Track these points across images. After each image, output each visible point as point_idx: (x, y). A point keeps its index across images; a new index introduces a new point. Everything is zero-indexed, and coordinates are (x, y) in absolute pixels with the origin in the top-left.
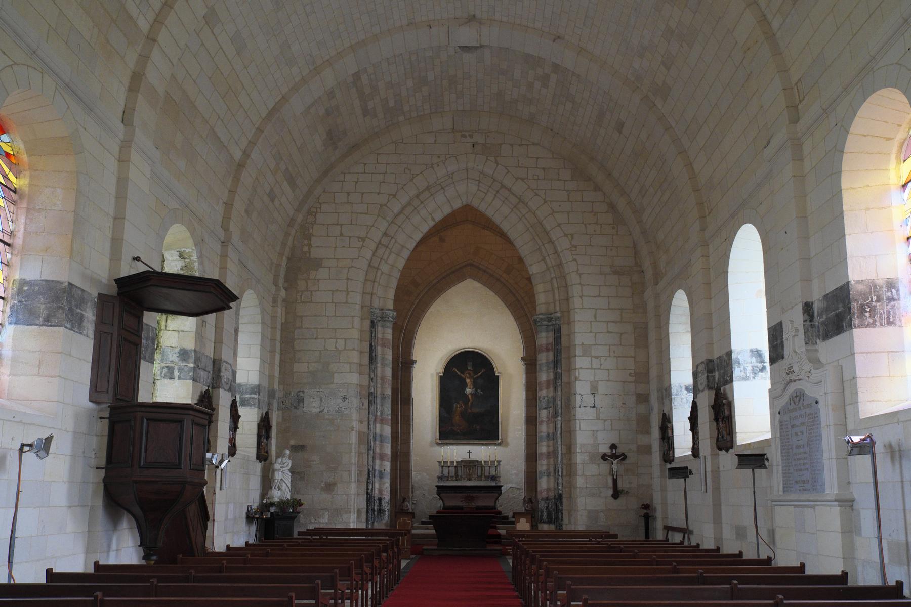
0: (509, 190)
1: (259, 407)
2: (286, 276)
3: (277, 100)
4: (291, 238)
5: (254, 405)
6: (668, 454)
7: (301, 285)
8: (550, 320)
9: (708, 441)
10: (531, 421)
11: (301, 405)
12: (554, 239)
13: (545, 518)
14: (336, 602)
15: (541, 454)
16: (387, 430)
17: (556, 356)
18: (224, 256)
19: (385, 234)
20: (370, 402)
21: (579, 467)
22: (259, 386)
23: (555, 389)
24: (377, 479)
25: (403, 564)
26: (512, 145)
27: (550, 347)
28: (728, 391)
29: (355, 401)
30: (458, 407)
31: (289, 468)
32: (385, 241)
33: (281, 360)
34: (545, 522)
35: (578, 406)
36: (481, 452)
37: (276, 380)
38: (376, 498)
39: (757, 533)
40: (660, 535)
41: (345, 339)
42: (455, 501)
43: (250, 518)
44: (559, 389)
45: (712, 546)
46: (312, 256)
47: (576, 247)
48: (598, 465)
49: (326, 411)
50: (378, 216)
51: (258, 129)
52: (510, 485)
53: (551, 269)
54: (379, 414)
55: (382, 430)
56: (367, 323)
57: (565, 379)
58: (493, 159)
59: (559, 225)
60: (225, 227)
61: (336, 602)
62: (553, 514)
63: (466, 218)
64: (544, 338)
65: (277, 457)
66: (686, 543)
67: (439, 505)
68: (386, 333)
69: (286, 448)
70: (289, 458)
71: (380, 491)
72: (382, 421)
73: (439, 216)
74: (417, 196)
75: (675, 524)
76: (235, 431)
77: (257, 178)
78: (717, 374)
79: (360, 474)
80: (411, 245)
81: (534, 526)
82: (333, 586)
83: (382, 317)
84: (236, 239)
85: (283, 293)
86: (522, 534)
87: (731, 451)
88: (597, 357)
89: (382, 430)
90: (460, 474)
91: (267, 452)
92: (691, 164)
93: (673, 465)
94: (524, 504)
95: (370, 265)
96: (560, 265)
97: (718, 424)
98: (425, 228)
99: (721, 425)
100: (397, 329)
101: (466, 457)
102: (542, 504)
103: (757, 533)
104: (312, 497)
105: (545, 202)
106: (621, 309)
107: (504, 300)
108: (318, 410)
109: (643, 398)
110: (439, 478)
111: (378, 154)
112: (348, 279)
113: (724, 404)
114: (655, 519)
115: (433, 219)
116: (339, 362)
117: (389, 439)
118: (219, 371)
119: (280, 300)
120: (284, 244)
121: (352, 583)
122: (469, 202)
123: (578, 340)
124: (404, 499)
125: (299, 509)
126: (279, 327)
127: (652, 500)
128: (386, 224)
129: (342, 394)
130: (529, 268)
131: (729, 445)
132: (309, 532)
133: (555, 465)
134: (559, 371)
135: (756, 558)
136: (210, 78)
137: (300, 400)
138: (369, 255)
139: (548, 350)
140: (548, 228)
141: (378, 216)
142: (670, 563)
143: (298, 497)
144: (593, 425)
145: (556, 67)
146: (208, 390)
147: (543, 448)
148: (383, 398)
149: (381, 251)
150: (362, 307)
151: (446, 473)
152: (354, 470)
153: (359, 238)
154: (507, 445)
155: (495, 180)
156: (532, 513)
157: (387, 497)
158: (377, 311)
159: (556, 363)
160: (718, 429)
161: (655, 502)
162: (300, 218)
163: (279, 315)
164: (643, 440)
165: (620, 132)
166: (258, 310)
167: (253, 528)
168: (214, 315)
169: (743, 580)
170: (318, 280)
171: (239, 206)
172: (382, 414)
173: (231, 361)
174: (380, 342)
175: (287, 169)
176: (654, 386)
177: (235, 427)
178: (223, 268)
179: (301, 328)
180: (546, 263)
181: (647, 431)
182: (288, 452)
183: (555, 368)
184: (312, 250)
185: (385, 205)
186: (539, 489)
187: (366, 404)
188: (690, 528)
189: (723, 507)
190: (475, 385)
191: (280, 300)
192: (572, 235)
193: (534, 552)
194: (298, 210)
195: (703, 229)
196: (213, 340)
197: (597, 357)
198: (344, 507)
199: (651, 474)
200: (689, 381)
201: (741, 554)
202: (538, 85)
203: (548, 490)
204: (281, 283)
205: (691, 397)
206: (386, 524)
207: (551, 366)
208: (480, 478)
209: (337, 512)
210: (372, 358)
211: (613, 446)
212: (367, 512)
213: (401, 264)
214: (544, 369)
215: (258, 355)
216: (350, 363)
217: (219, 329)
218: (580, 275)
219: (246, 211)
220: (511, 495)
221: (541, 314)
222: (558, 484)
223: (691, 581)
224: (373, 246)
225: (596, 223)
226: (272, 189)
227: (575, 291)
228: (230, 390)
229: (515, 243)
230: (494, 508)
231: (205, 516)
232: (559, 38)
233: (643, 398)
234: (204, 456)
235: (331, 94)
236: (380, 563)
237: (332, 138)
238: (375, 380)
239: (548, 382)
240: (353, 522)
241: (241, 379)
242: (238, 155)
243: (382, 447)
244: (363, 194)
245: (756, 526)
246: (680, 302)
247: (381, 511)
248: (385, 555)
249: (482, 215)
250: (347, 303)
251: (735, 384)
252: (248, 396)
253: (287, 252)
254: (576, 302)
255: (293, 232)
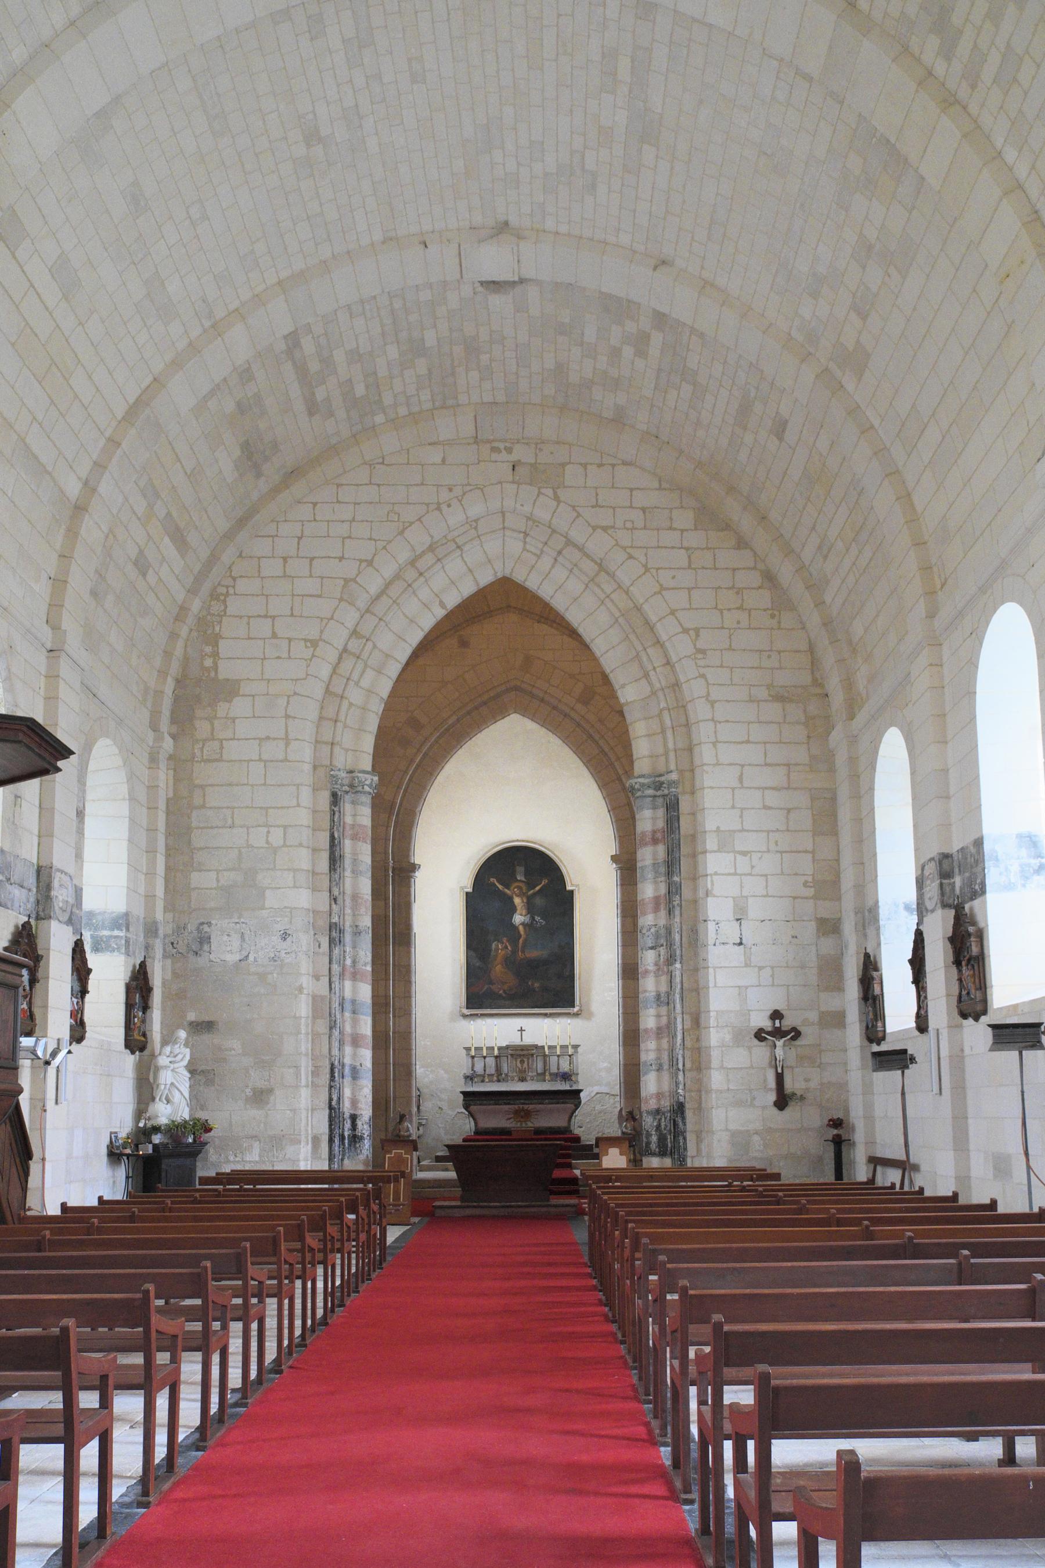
0: (581, 549)
1: (127, 954)
2: (173, 712)
3: (144, 386)
4: (180, 644)
5: (119, 949)
6: (874, 1026)
7: (202, 728)
8: (659, 786)
9: (944, 1001)
10: (630, 972)
11: (206, 947)
12: (664, 637)
13: (653, 1146)
14: (246, 1302)
15: (646, 1030)
16: (365, 992)
17: (670, 852)
18: (52, 677)
19: (355, 633)
20: (331, 941)
21: (715, 1054)
22: (127, 914)
23: (670, 912)
24: (348, 1080)
25: (393, 1234)
26: (585, 466)
27: (659, 835)
28: (977, 911)
29: (304, 940)
30: (500, 948)
31: (185, 1062)
32: (354, 645)
33: (168, 869)
34: (653, 1154)
35: (711, 942)
36: (541, 1029)
37: (160, 905)
38: (347, 1115)
39: (1029, 1167)
40: (862, 1173)
41: (285, 827)
42: (498, 1119)
43: (114, 1155)
44: (677, 912)
45: (946, 1191)
46: (221, 677)
47: (703, 652)
48: (750, 1048)
49: (251, 958)
50: (341, 600)
51: (110, 440)
52: (596, 1089)
53: (660, 694)
54: (348, 962)
55: (355, 990)
56: (325, 797)
57: (686, 893)
58: (549, 492)
59: (673, 612)
60: (53, 623)
61: (246, 1302)
62: (669, 1139)
63: (503, 603)
64: (649, 819)
65: (165, 1042)
66: (906, 1188)
67: (467, 1126)
68: (360, 815)
69: (178, 1027)
70: (186, 1045)
71: (354, 1102)
72: (355, 976)
73: (452, 600)
74: (412, 563)
75: (889, 1155)
76: (83, 997)
77: (111, 531)
78: (958, 881)
79: (315, 1073)
80: (403, 654)
81: (635, 1162)
82: (240, 1271)
83: (351, 786)
84: (73, 642)
85: (168, 744)
86: (608, 1177)
87: (983, 1019)
88: (744, 853)
89: (355, 990)
90: (505, 1069)
91: (144, 1035)
92: (909, 495)
93: (884, 1047)
94: (620, 1124)
95: (327, 691)
96: (676, 686)
97: (960, 971)
98: (428, 622)
99: (966, 972)
100: (381, 806)
101: (515, 1039)
102: (648, 1122)
103: (1029, 1167)
104: (228, 1116)
105: (647, 570)
106: (788, 765)
107: (579, 750)
108: (237, 957)
109: (830, 927)
110: (466, 1077)
111: (338, 485)
112: (287, 717)
113: (969, 935)
114: (852, 1144)
115: (442, 604)
116: (274, 869)
117: (368, 1010)
118: (49, 887)
119: (162, 757)
120: (167, 654)
121: (280, 1268)
122: (507, 573)
123: (711, 821)
124: (402, 1117)
125: (205, 1137)
126: (162, 805)
127: (847, 1111)
128: (357, 615)
129: (280, 927)
130: (619, 694)
131: (979, 1008)
132: (221, 1178)
133: (672, 1050)
134: (676, 879)
135: (1027, 1210)
136: (13, 344)
137: (204, 940)
138: (325, 672)
139: (655, 841)
140: (653, 618)
141: (341, 600)
142: (857, 1222)
143: (202, 1115)
144: (740, 973)
145: (660, 319)
146: (28, 923)
147: (649, 1020)
148: (357, 933)
149: (347, 664)
150: (315, 767)
151: (479, 1068)
152: (305, 1065)
153: (306, 640)
154: (590, 1016)
155: (554, 531)
156: (632, 1141)
157: (366, 1112)
158: (343, 774)
159: (671, 865)
160: (960, 980)
161: (853, 1114)
162: (196, 605)
163: (162, 785)
164: (830, 1002)
165: (781, 439)
166: (122, 776)
167: (121, 1172)
168: (35, 782)
169: (979, 1250)
170: (234, 720)
171: (79, 582)
172: (354, 962)
173: (71, 869)
174: (349, 832)
175: (169, 514)
176: (848, 903)
177: (81, 991)
178: (51, 699)
179: (203, 806)
180: (650, 683)
181: (838, 987)
182: (182, 1034)
183: (669, 874)
184: (221, 664)
185: (354, 580)
186: (643, 1094)
187: (325, 942)
188: (913, 1159)
189: (970, 1121)
190: (530, 909)
191: (162, 757)
192: (697, 631)
193: (618, 1206)
194: (193, 591)
195: (931, 615)
196: (36, 832)
197: (744, 853)
198: (283, 1129)
199: (846, 1064)
200: (911, 894)
201: (993, 1204)
202: (628, 351)
203: (659, 1096)
204: (165, 725)
205: (914, 919)
206: (366, 1163)
207: (663, 869)
208: (541, 1077)
209: (277, 1142)
210: (335, 860)
211: (776, 1015)
212: (331, 1141)
213: (385, 688)
214: (650, 876)
215: (124, 857)
216: (295, 870)
217: (46, 811)
218: (713, 703)
219: (94, 593)
220: (598, 1107)
221: (643, 776)
222: (677, 1084)
223: (896, 1252)
224: (332, 656)
225: (741, 608)
226: (141, 552)
227: (704, 732)
228: (70, 922)
229: (592, 646)
230: (567, 1130)
231: (23, 1151)
232: (664, 262)
233: (830, 927)
234: (15, 1042)
235: (246, 374)
236: (341, 1231)
237: (252, 456)
238: (340, 901)
239: (657, 899)
240: (306, 1156)
241: (89, 903)
242: (73, 488)
243: (355, 1023)
244: (312, 559)
245: (1027, 1154)
246: (893, 750)
247: (355, 1139)
248: (352, 1217)
249: (535, 598)
250: (286, 760)
251: (990, 896)
252: (106, 933)
253: (175, 668)
254: (706, 754)
255: (184, 631)
